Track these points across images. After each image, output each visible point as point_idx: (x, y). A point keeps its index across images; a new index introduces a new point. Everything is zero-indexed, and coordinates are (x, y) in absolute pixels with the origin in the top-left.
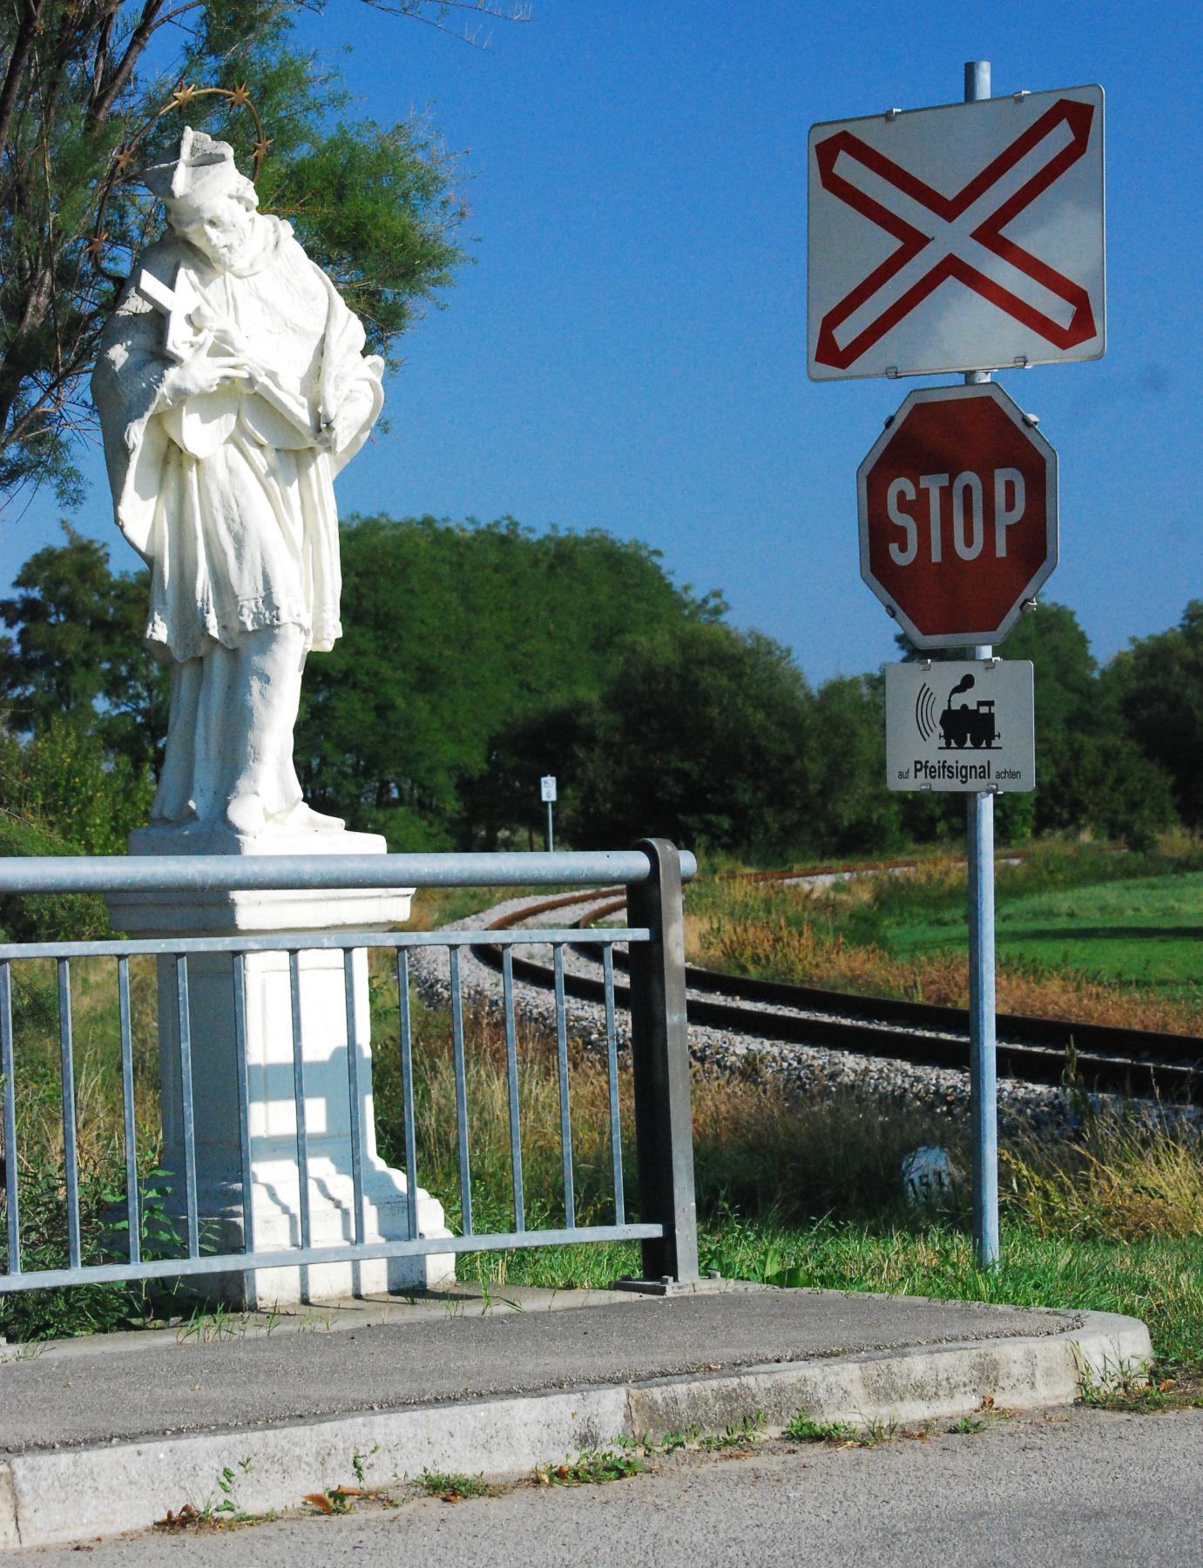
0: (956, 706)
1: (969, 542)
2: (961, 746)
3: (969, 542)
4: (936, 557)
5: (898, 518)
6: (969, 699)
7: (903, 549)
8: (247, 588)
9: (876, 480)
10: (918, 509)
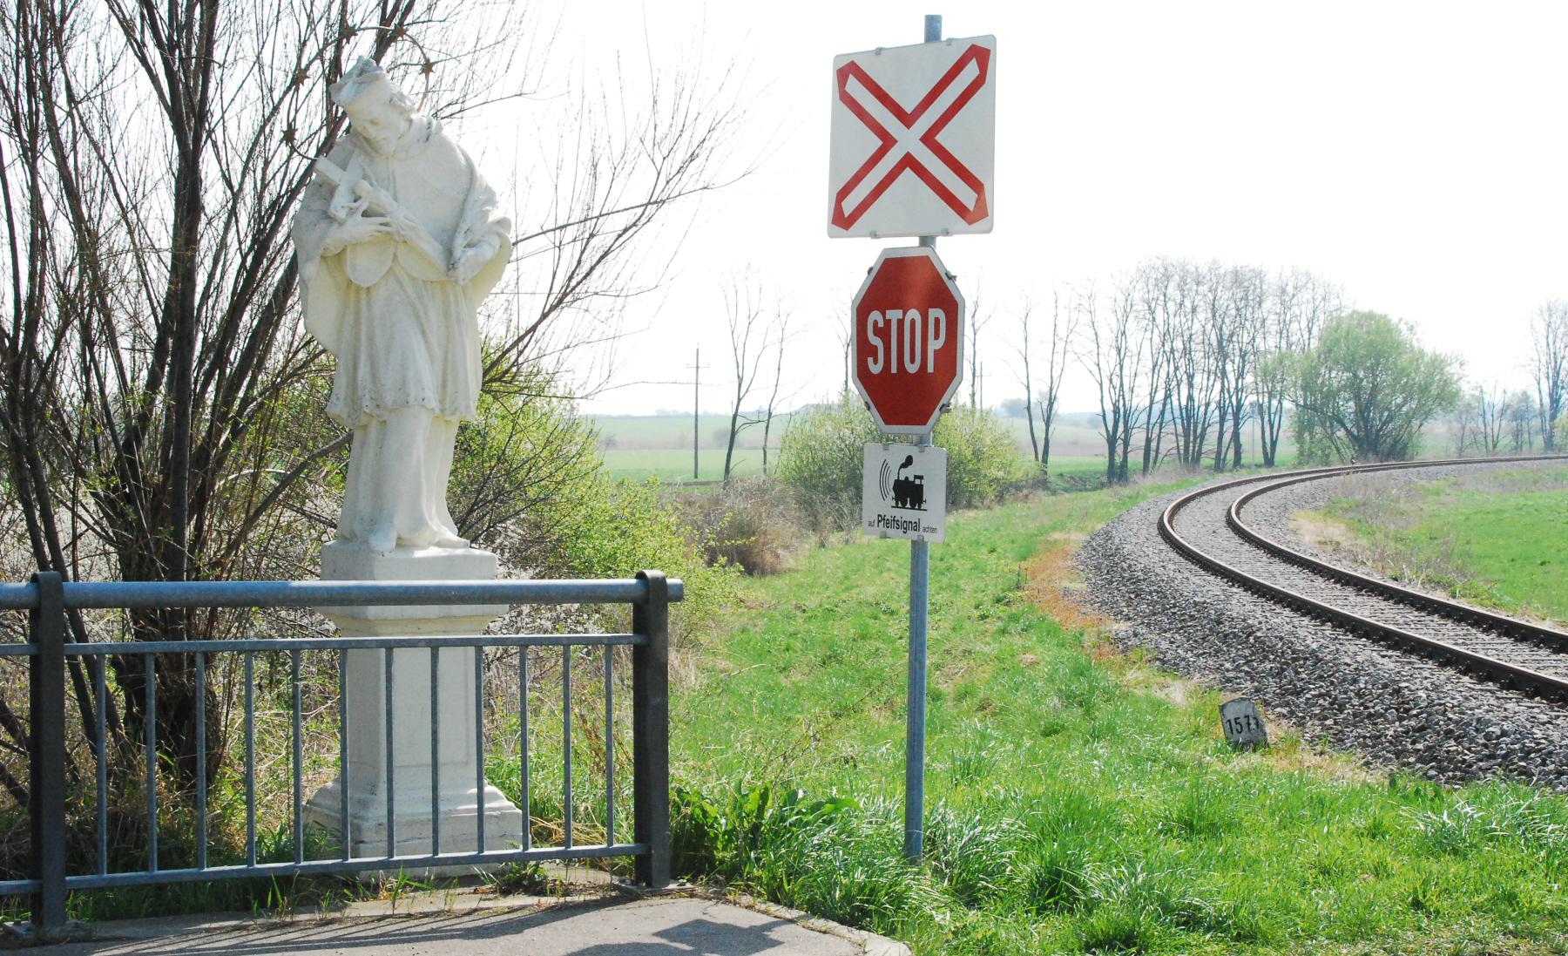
0: (902, 478)
1: (912, 361)
2: (904, 507)
3: (912, 361)
4: (894, 370)
5: (875, 341)
6: (909, 473)
7: (876, 362)
8: (389, 379)
9: (862, 311)
10: (883, 333)
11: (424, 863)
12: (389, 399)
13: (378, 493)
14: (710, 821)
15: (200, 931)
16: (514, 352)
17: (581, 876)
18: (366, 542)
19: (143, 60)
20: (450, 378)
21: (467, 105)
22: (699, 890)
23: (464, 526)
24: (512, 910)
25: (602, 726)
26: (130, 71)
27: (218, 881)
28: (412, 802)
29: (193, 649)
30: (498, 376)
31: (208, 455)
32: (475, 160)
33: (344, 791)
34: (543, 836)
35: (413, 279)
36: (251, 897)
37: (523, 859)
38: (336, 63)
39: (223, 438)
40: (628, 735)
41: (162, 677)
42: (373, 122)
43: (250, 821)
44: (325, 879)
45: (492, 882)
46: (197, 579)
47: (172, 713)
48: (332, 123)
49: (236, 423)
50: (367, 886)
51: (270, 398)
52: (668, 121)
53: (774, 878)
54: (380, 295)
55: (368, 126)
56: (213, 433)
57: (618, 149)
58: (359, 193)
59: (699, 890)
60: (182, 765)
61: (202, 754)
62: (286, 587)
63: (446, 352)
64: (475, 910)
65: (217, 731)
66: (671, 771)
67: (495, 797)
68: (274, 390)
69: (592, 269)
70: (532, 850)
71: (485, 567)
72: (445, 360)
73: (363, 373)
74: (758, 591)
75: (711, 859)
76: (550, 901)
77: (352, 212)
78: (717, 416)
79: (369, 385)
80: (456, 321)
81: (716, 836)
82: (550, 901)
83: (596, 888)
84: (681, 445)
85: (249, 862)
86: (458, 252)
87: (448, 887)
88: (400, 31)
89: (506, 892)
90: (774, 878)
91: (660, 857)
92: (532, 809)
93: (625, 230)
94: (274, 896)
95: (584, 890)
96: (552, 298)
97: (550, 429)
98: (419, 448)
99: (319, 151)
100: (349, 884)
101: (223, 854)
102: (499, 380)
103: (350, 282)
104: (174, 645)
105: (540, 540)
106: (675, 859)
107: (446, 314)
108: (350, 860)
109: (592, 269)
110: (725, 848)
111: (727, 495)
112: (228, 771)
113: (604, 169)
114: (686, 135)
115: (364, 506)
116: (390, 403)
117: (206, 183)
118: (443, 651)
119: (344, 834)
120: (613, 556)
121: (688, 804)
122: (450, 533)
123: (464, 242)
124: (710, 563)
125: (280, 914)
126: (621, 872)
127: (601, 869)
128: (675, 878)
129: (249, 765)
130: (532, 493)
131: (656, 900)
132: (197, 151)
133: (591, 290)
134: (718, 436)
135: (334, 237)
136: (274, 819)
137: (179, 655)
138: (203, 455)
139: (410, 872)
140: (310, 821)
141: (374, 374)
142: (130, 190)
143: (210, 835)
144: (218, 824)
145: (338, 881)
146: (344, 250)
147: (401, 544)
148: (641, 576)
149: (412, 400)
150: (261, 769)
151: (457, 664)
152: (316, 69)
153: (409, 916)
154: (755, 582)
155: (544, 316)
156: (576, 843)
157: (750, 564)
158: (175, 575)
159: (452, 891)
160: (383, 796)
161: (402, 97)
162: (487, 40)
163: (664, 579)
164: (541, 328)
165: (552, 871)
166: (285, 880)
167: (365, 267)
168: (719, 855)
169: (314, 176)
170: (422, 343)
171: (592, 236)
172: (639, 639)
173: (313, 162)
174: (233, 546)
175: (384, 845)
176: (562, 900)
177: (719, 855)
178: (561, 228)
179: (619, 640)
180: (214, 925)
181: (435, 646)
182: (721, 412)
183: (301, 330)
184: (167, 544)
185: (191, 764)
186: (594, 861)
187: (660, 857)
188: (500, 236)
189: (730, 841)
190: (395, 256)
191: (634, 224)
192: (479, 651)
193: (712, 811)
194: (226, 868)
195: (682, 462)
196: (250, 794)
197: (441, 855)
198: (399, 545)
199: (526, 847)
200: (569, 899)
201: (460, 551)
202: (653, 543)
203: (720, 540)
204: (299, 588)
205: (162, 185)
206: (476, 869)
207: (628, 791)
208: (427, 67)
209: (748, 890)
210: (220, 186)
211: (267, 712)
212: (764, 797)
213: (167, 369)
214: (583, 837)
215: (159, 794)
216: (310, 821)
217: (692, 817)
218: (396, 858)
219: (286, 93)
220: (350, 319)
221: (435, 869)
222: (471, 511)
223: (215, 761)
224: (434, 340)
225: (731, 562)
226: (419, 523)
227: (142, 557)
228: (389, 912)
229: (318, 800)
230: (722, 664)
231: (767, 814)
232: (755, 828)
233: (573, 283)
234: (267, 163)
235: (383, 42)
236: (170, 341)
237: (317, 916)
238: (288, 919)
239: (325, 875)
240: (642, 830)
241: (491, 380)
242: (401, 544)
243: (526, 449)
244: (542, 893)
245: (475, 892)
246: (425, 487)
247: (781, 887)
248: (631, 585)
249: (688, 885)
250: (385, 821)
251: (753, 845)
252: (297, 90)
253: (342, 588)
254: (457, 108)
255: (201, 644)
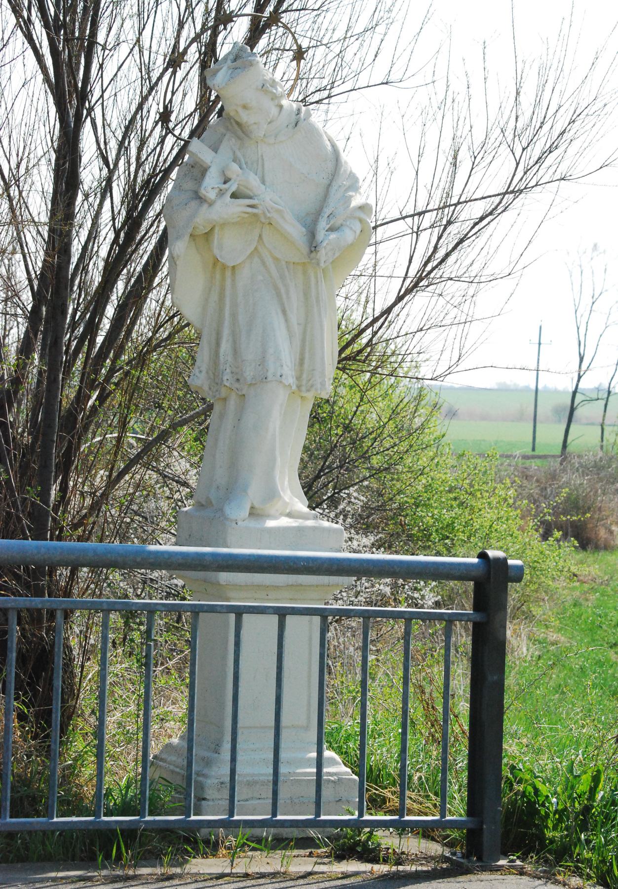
8: (250, 354)
11: (262, 824)
12: (249, 373)
13: (234, 465)
14: (541, 799)
15: (47, 879)
16: (369, 331)
17: (413, 845)
18: (221, 510)
19: (29, 37)
20: (307, 355)
21: (335, 91)
22: (529, 868)
23: (314, 503)
24: (346, 876)
25: (438, 696)
26: (19, 50)
27: (66, 832)
28: (254, 763)
29: (54, 606)
30: (353, 356)
31: (76, 419)
32: (340, 145)
33: (190, 749)
34: (377, 803)
35: (276, 259)
36: (97, 849)
37: (358, 825)
38: (211, 47)
39: (90, 403)
40: (463, 707)
41: (23, 630)
42: (245, 107)
43: (100, 774)
44: (166, 832)
45: (327, 845)
46: (59, 538)
47: (30, 667)
48: (205, 106)
49: (103, 390)
50: (207, 842)
51: (136, 368)
52: (528, 114)
53: (603, 861)
54: (244, 274)
55: (240, 110)
56: (81, 398)
57: (479, 137)
58: (229, 174)
59: (529, 868)
60: (37, 715)
61: (57, 705)
62: (144, 551)
63: (304, 333)
64: (310, 874)
65: (72, 685)
66: (505, 746)
67: (333, 762)
68: (141, 360)
69: (447, 255)
70: (367, 817)
71: (330, 537)
72: (303, 341)
73: (225, 347)
74: (592, 566)
75: (541, 838)
76: (382, 869)
77: (221, 193)
78: (556, 391)
79: (230, 358)
80: (313, 302)
81: (547, 815)
82: (382, 869)
83: (428, 858)
84: (520, 418)
85: (96, 814)
86: (321, 234)
87: (285, 848)
88: (275, 19)
89: (340, 858)
90: (603, 861)
91: (491, 832)
92: (368, 775)
93: (482, 219)
94: (119, 848)
95: (416, 860)
96: (408, 281)
97: (396, 401)
98: (275, 422)
99: (192, 134)
100: (189, 841)
101: (73, 805)
102: (354, 359)
103: (216, 261)
104: (36, 602)
105: (381, 508)
106: (506, 834)
107: (306, 294)
108: (193, 818)
109: (447, 255)
110: (555, 828)
111: (564, 470)
112: (80, 723)
113: (465, 158)
114: (546, 127)
115: (221, 476)
116: (249, 378)
117: (84, 160)
118: (289, 618)
119: (188, 791)
120: (450, 526)
121: (520, 782)
122: (301, 505)
123: (327, 223)
124: (545, 537)
125: (123, 867)
126: (451, 845)
127: (433, 839)
128: (505, 854)
129: (101, 721)
130: (376, 461)
131: (485, 876)
132: (79, 123)
133: (446, 275)
134: (557, 411)
135: (204, 217)
136: (122, 773)
137: (39, 611)
138: (70, 418)
139: (249, 832)
140: (156, 777)
141: (236, 351)
142: (13, 166)
143: (61, 785)
144: (70, 773)
145: (179, 837)
146: (212, 229)
147: (254, 513)
148: (483, 556)
149: (270, 375)
150: (112, 720)
151: (303, 633)
152: (193, 54)
153: (246, 876)
154: (589, 556)
155: (399, 299)
156: (410, 812)
157: (584, 538)
158: (39, 535)
159: (288, 853)
160: (226, 755)
161: (274, 83)
162: (358, 29)
163: (505, 560)
164: (396, 309)
165: (387, 840)
166: (130, 834)
167: (232, 247)
168: (549, 834)
169: (187, 157)
170: (282, 320)
171: (449, 223)
172: (478, 617)
173: (187, 143)
174: (95, 507)
175: (226, 803)
176: (394, 868)
177: (549, 834)
178: (419, 214)
179: (459, 617)
180: (61, 874)
181: (282, 614)
182: (560, 388)
183: (168, 303)
184: (33, 503)
185: (45, 716)
186: (426, 831)
187: (491, 832)
188: (361, 221)
189: (560, 820)
190: (260, 236)
191: (491, 213)
192: (324, 619)
193: (544, 789)
194: (75, 819)
195: (521, 434)
196: (100, 748)
197: (279, 817)
198: (251, 514)
199: (361, 814)
200: (401, 868)
201: (310, 523)
202: (490, 515)
203: (556, 514)
204: (157, 553)
205: (43, 161)
206: (312, 833)
207: (462, 762)
208: (299, 55)
209: (577, 872)
210: (98, 163)
211: (121, 666)
212: (596, 779)
213: (40, 336)
214: (415, 806)
215: (14, 742)
216: (156, 777)
217: (524, 794)
218: (236, 818)
219: (165, 70)
220: (214, 297)
221: (272, 830)
222: (318, 477)
223: (69, 714)
224: (294, 319)
225: (565, 536)
226: (272, 494)
227: (8, 513)
228: (228, 871)
229: (163, 756)
230: (553, 636)
231: (599, 796)
232: (587, 810)
233: (429, 268)
234: (143, 143)
235: (256, 32)
236: (44, 309)
237: (158, 871)
238: (131, 872)
239: (167, 830)
240: (474, 806)
241: (346, 359)
242: (254, 513)
243: (372, 420)
244: (375, 860)
245: (311, 855)
246: (279, 460)
247: (610, 871)
248: (472, 565)
249: (518, 863)
250: (227, 779)
251: (584, 827)
252: (174, 73)
253: (197, 554)
254: (326, 94)
255: (60, 601)
